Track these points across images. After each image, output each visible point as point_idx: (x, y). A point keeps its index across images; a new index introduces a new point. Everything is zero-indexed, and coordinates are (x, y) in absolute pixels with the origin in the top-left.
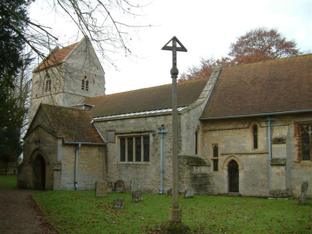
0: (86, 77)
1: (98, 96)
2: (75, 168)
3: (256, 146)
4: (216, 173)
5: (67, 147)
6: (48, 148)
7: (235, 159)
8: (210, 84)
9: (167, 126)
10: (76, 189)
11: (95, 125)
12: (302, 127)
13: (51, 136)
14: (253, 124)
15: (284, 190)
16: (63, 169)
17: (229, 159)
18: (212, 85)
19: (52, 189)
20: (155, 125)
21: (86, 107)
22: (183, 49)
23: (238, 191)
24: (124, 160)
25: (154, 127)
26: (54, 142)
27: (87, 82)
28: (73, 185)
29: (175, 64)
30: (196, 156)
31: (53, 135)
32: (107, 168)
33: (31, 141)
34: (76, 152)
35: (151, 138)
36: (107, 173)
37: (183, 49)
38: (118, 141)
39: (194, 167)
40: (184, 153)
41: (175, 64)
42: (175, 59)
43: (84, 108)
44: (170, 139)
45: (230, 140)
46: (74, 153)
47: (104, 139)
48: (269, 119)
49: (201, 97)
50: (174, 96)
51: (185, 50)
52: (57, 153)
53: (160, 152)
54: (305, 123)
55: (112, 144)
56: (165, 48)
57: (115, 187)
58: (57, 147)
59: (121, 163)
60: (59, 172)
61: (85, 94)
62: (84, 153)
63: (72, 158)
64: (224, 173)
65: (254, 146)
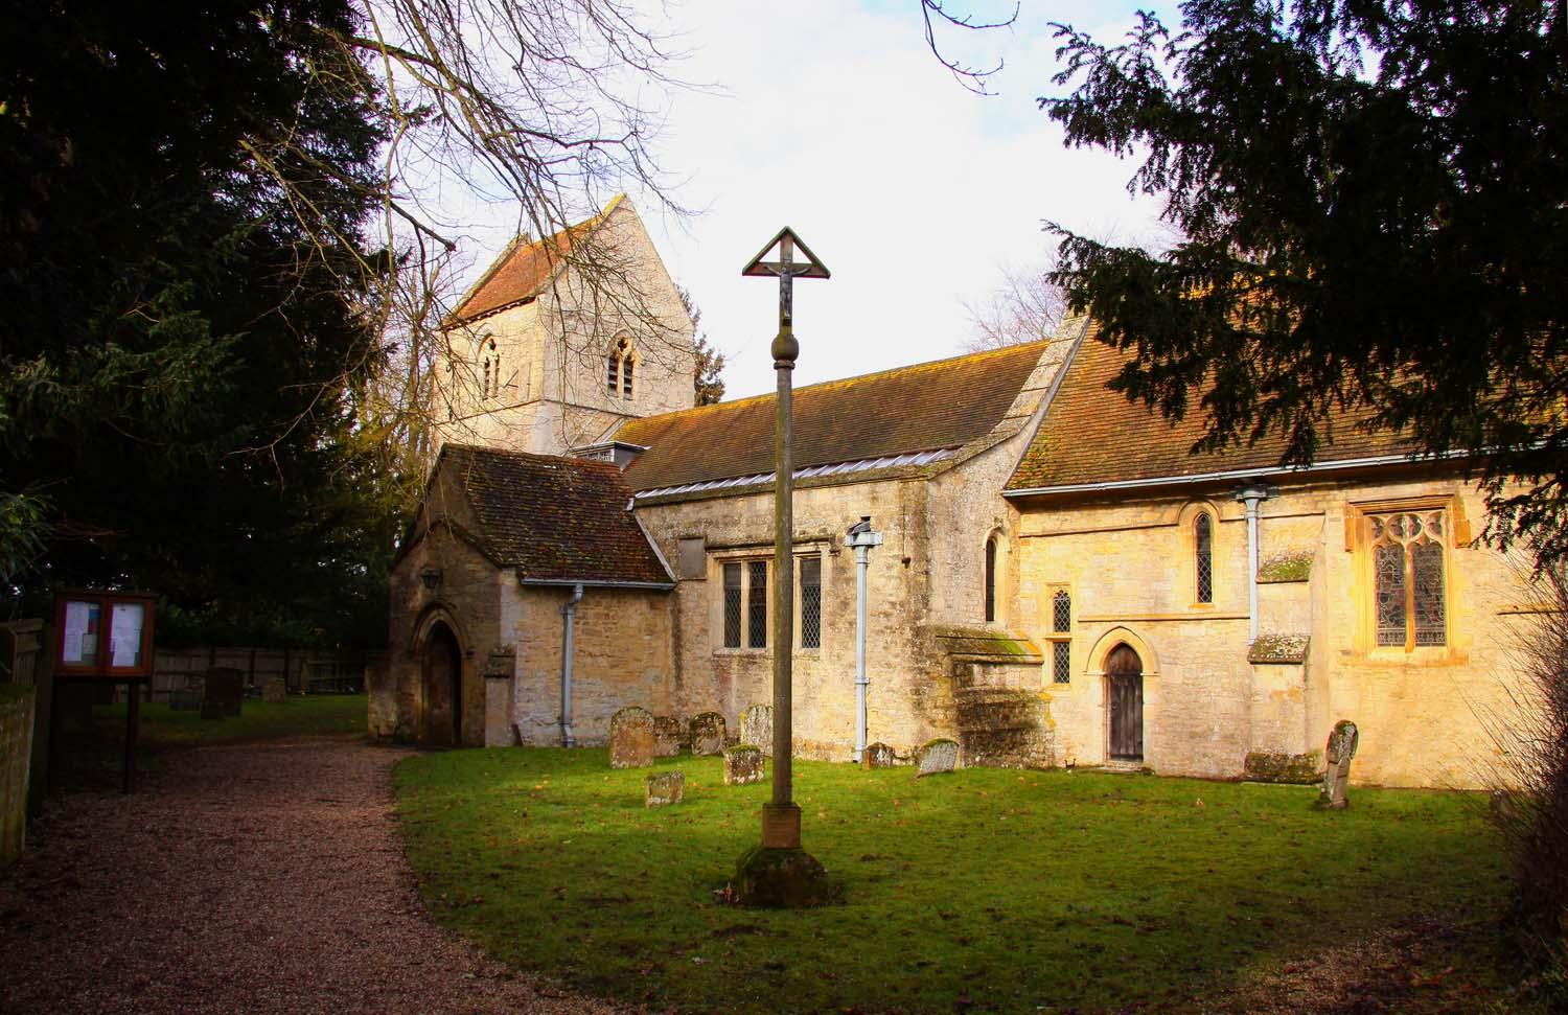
0: (622, 345)
1: (668, 410)
2: (563, 669)
3: (1205, 594)
4: (1061, 692)
5: (534, 599)
6: (468, 600)
7: (1131, 641)
8: (1048, 365)
9: (880, 520)
10: (565, 744)
11: (637, 518)
12: (1377, 521)
13: (477, 558)
14: (1193, 509)
15: (1298, 757)
16: (518, 673)
17: (1111, 641)
18: (1055, 368)
19: (482, 745)
20: (838, 519)
21: (623, 453)
22: (817, 270)
23: (1141, 757)
24: (738, 644)
25: (836, 526)
26: (489, 581)
27: (629, 363)
28: (556, 729)
29: (786, 323)
30: (990, 627)
31: (485, 555)
32: (679, 668)
33: (413, 576)
34: (565, 616)
35: (827, 562)
36: (680, 686)
37: (817, 270)
38: (715, 573)
39: (976, 668)
40: (941, 618)
41: (786, 323)
42: (786, 304)
43: (611, 457)
44: (889, 567)
45: (1113, 570)
46: (560, 619)
47: (668, 569)
48: (1251, 493)
49: (1011, 412)
50: (783, 433)
51: (826, 274)
52: (497, 618)
53: (855, 611)
54: (1384, 506)
55: (696, 585)
56: (755, 268)
57: (692, 737)
58: (498, 596)
59: (727, 651)
60: (504, 683)
61: (618, 403)
62: (597, 616)
63: (554, 635)
64: (1088, 693)
65: (1201, 593)
